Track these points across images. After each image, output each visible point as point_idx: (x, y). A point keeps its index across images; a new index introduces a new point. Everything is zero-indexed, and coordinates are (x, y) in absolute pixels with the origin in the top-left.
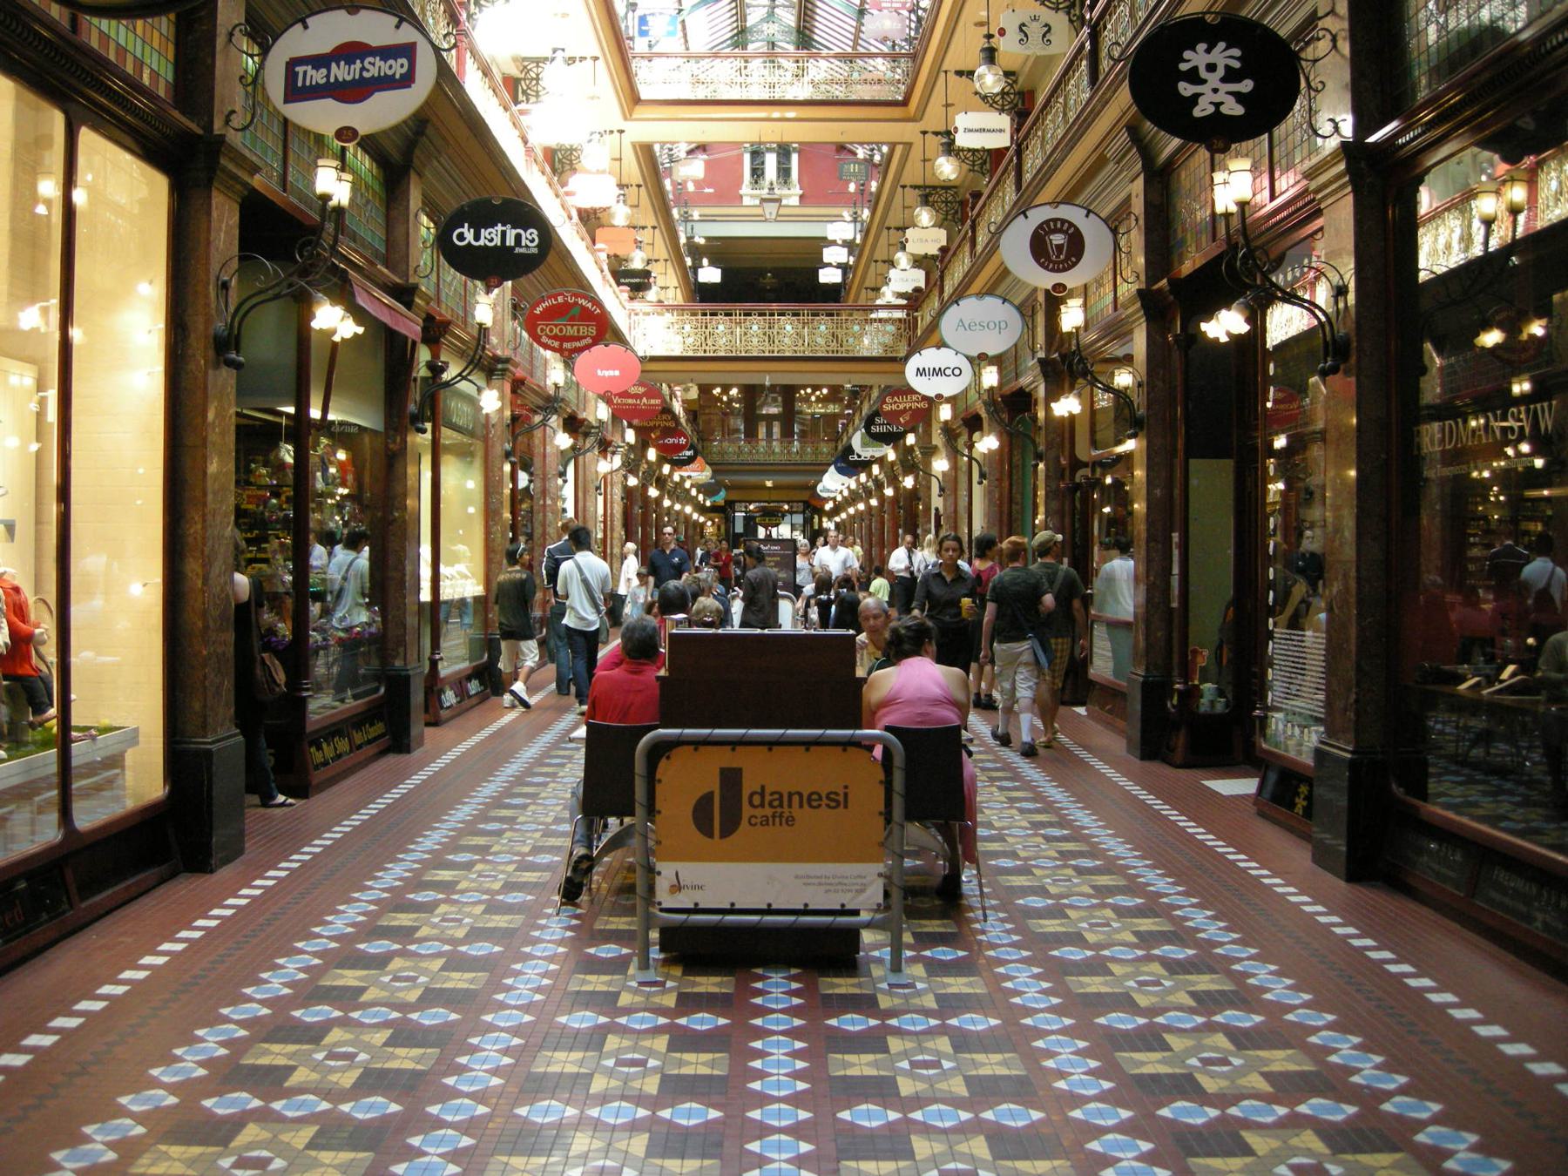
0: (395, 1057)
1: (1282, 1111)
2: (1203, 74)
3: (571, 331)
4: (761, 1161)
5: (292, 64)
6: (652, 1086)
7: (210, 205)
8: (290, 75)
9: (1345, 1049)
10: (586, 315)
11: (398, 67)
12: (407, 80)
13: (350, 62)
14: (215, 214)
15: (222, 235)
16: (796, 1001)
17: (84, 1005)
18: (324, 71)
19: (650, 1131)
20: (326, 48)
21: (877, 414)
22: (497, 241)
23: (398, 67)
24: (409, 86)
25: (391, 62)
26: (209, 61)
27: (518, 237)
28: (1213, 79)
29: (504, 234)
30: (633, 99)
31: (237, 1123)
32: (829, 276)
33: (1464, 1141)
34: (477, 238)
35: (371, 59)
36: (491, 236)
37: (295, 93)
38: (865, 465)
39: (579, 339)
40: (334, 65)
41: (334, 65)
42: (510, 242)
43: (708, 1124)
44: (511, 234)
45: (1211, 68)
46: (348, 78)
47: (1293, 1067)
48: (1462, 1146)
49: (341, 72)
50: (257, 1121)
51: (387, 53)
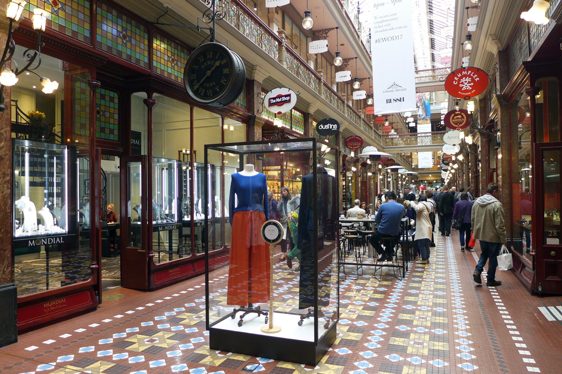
0: (350, 335)
2: (464, 83)
3: (355, 144)
4: (356, 368)
5: (270, 99)
6: (429, 324)
8: (270, 101)
10: (358, 141)
11: (288, 98)
12: (289, 101)
13: (279, 98)
14: (255, 130)
16: (464, 306)
19: (407, 354)
22: (328, 128)
23: (288, 98)
24: (30, 200)
27: (333, 126)
28: (466, 84)
30: (206, 147)
34: (324, 127)
36: (327, 127)
37: (271, 105)
39: (357, 146)
42: (331, 128)
43: (389, 354)
44: (331, 126)
45: (466, 82)
49: (278, 100)
51: (286, 96)
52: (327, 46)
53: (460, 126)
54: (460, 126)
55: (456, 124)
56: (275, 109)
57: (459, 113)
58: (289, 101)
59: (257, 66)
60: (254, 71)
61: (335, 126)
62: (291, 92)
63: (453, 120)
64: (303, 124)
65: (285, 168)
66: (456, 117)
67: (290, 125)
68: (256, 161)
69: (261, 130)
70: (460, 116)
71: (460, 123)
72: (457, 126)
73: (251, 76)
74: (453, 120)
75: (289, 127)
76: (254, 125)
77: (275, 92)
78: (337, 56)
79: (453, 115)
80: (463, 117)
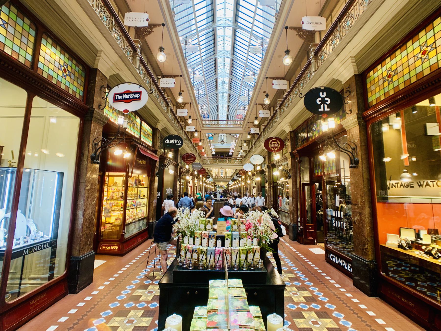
1: (291, 284)
3: (190, 160)
5: (116, 94)
7: (91, 125)
8: (115, 97)
9: (300, 274)
11: (137, 96)
12: (139, 99)
13: (127, 94)
14: (93, 128)
15: (96, 133)
17: (141, 256)
18: (121, 96)
20: (122, 91)
21: (238, 173)
22: (173, 142)
23: (137, 96)
25: (136, 95)
26: (93, 92)
27: (177, 142)
29: (175, 141)
31: (128, 311)
32: (230, 154)
33: (321, 298)
34: (170, 142)
35: (132, 94)
36: (172, 142)
37: (116, 100)
38: (236, 180)
39: (191, 161)
40: (124, 95)
41: (124, 95)
42: (176, 143)
46: (127, 98)
47: (292, 277)
48: (321, 297)
49: (125, 96)
50: (132, 309)
51: (135, 93)
52: (174, 83)
53: (276, 149)
54: (276, 149)
55: (273, 148)
56: (121, 106)
57: (275, 140)
58: (139, 99)
59: (102, 53)
60: (97, 58)
61: (179, 142)
62: (141, 89)
63: (271, 145)
64: (151, 137)
65: (130, 174)
66: (273, 143)
67: (139, 134)
68: (89, 164)
69: (101, 130)
70: (275, 142)
71: (276, 148)
72: (273, 149)
73: (94, 64)
74: (271, 145)
75: (138, 137)
76: (91, 121)
77: (122, 88)
78: (180, 95)
79: (271, 141)
80: (278, 143)
